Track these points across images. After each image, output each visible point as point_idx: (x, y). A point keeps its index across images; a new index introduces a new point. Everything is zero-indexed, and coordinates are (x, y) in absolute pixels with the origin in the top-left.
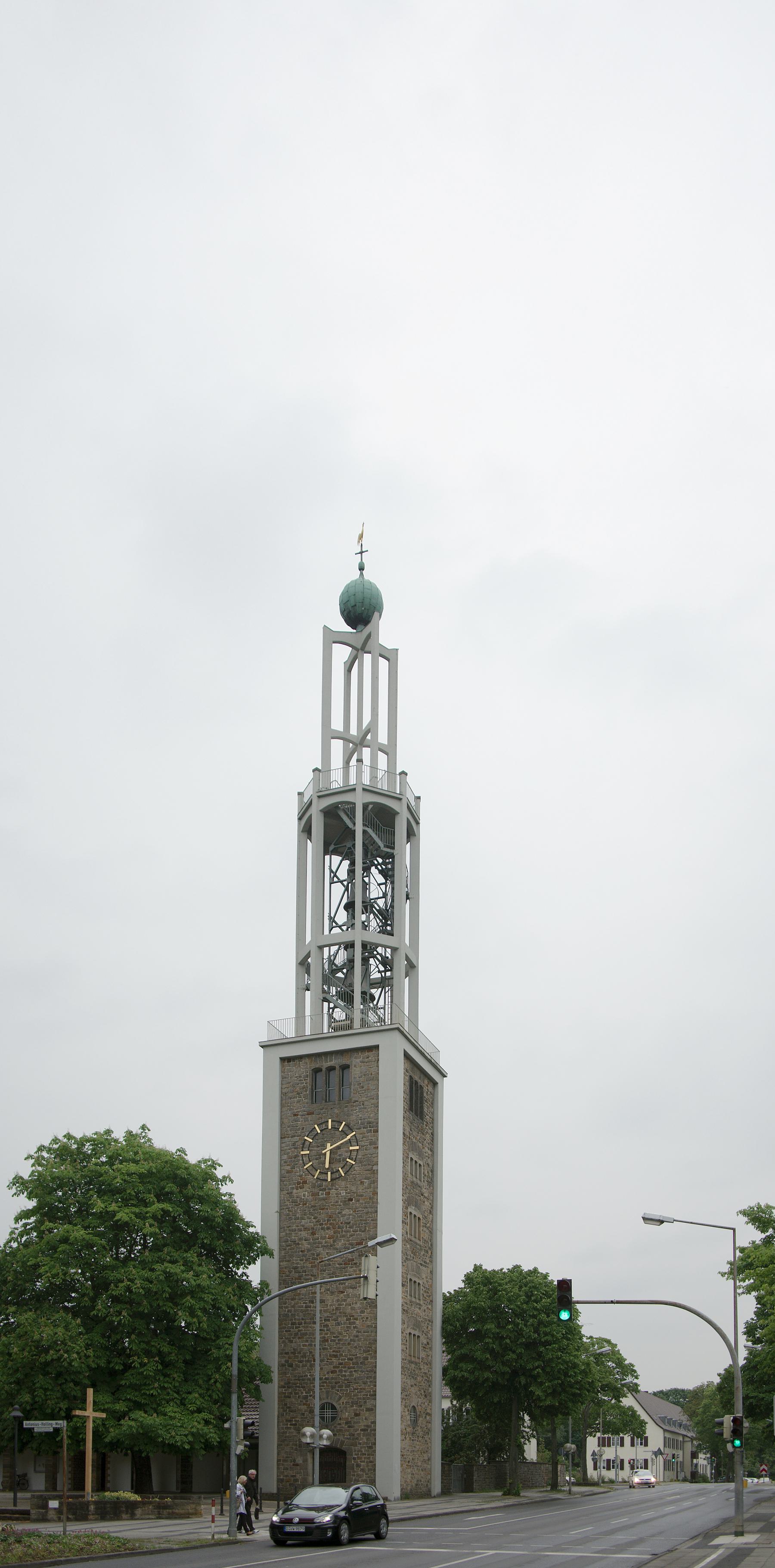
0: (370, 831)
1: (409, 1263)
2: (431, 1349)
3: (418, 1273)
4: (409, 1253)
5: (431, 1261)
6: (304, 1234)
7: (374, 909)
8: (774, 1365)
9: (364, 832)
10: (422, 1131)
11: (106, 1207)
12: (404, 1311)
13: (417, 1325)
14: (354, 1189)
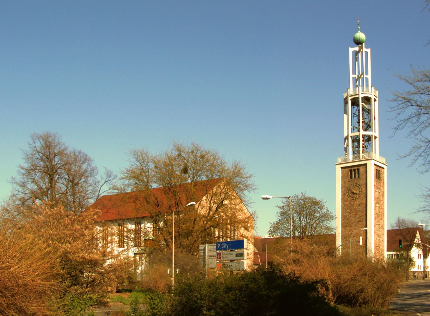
0: (363, 104)
1: (376, 220)
2: (383, 242)
3: (379, 222)
4: (376, 217)
5: (383, 218)
6: (348, 214)
7: (357, 62)
8: (3, 301)
9: (362, 105)
10: (380, 183)
12: (375, 233)
14: (361, 201)
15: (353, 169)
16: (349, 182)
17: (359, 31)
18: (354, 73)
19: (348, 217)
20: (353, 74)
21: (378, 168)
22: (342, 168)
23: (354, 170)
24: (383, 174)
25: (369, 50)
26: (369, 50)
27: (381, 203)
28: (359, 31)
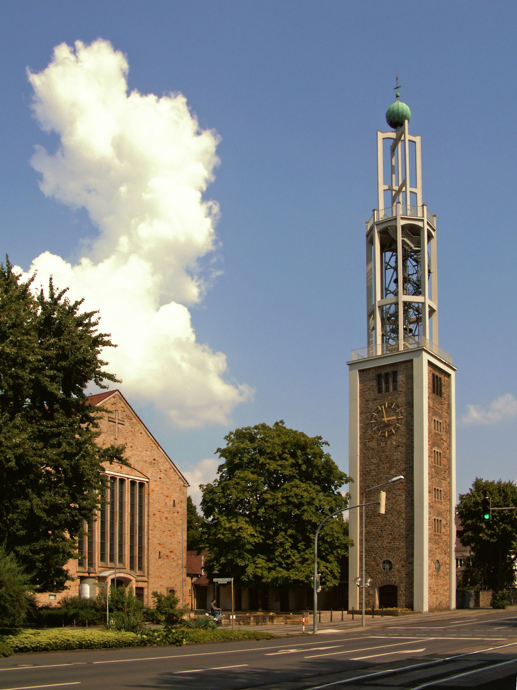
0: (406, 239)
1: (434, 479)
4: (434, 473)
7: (394, 176)
10: (441, 403)
13: (439, 514)
14: (400, 440)
15: (383, 372)
16: (375, 399)
18: (388, 181)
19: (374, 473)
21: (437, 373)
23: (387, 374)
24: (449, 386)
25: (418, 139)
26: (418, 139)
27: (443, 447)
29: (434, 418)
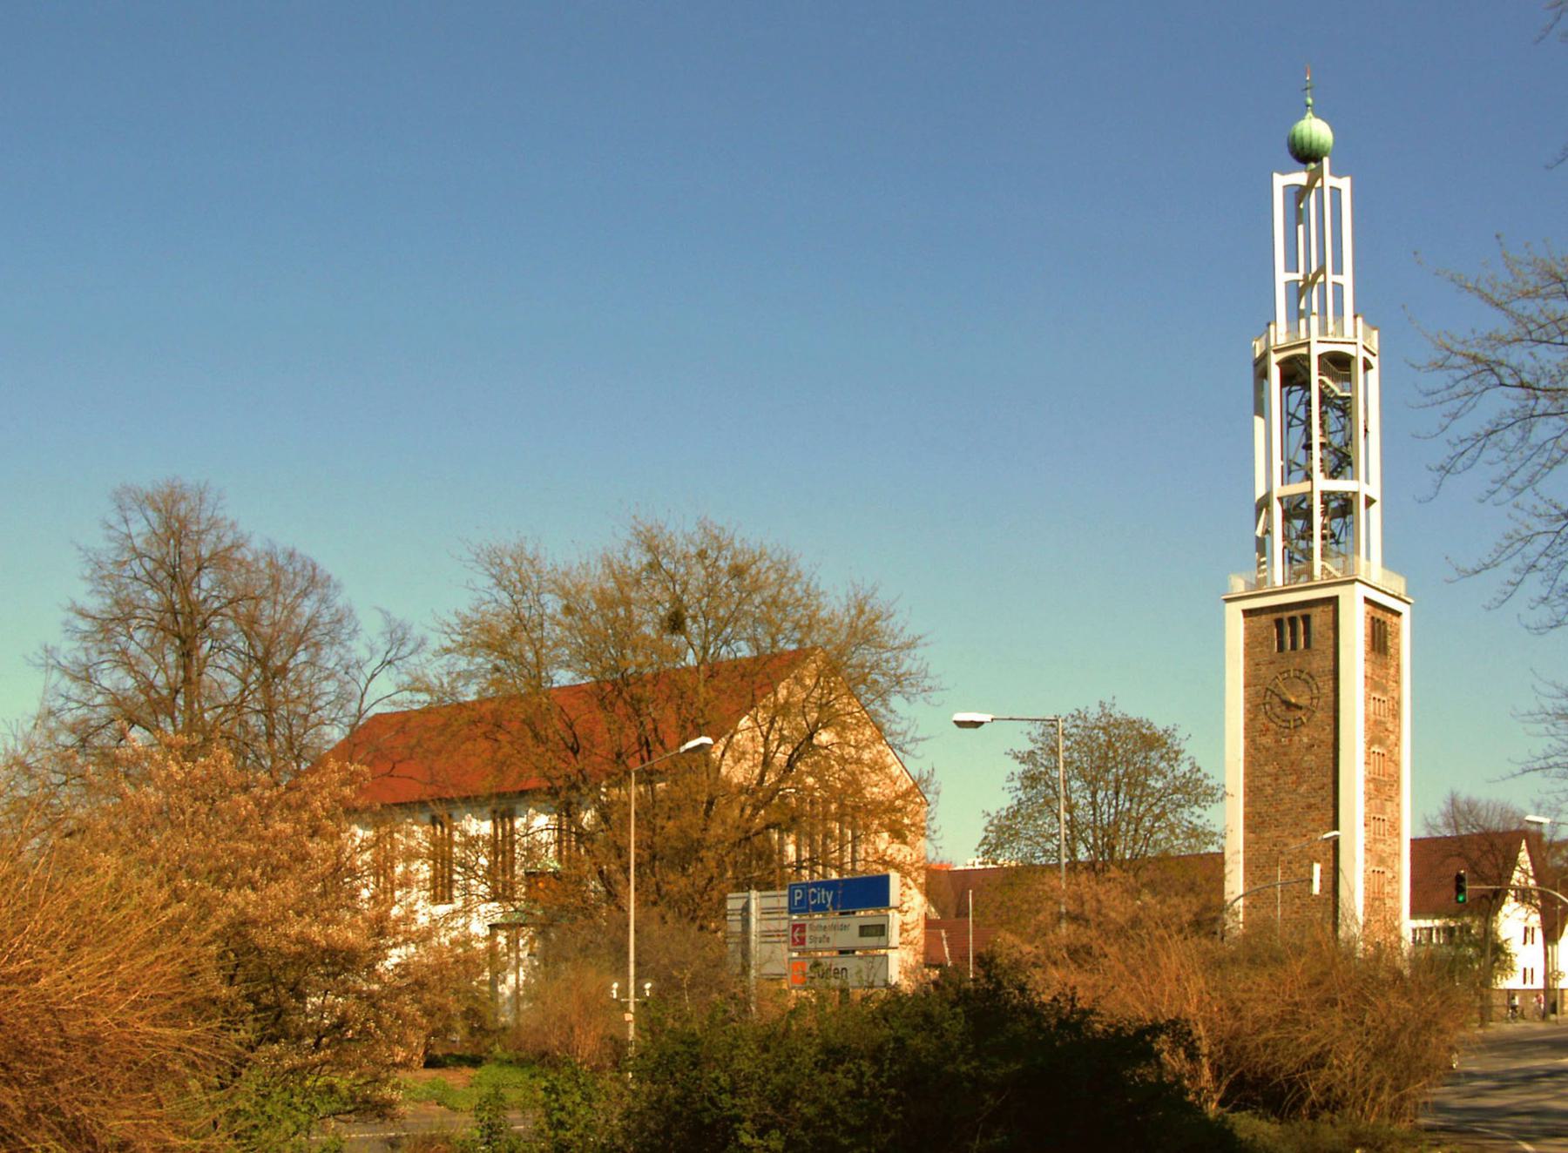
0: (1325, 379)
1: (1372, 802)
2: (1397, 882)
6: (1267, 780)
7: (1301, 228)
9: (1321, 382)
10: (1386, 666)
11: (1180, 931)
12: (1368, 850)
13: (1381, 861)
14: (1316, 735)
15: (1286, 615)
16: (1272, 663)
17: (1310, 114)
19: (1269, 791)
20: (1287, 270)
21: (1379, 614)
22: (1248, 613)
23: (1293, 620)
25: (1345, 184)
26: (1345, 184)
28: (1310, 114)
29: (1373, 695)
